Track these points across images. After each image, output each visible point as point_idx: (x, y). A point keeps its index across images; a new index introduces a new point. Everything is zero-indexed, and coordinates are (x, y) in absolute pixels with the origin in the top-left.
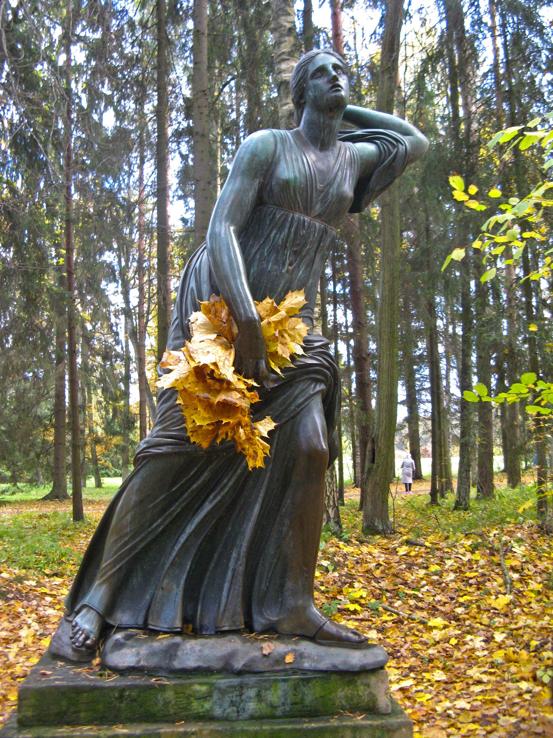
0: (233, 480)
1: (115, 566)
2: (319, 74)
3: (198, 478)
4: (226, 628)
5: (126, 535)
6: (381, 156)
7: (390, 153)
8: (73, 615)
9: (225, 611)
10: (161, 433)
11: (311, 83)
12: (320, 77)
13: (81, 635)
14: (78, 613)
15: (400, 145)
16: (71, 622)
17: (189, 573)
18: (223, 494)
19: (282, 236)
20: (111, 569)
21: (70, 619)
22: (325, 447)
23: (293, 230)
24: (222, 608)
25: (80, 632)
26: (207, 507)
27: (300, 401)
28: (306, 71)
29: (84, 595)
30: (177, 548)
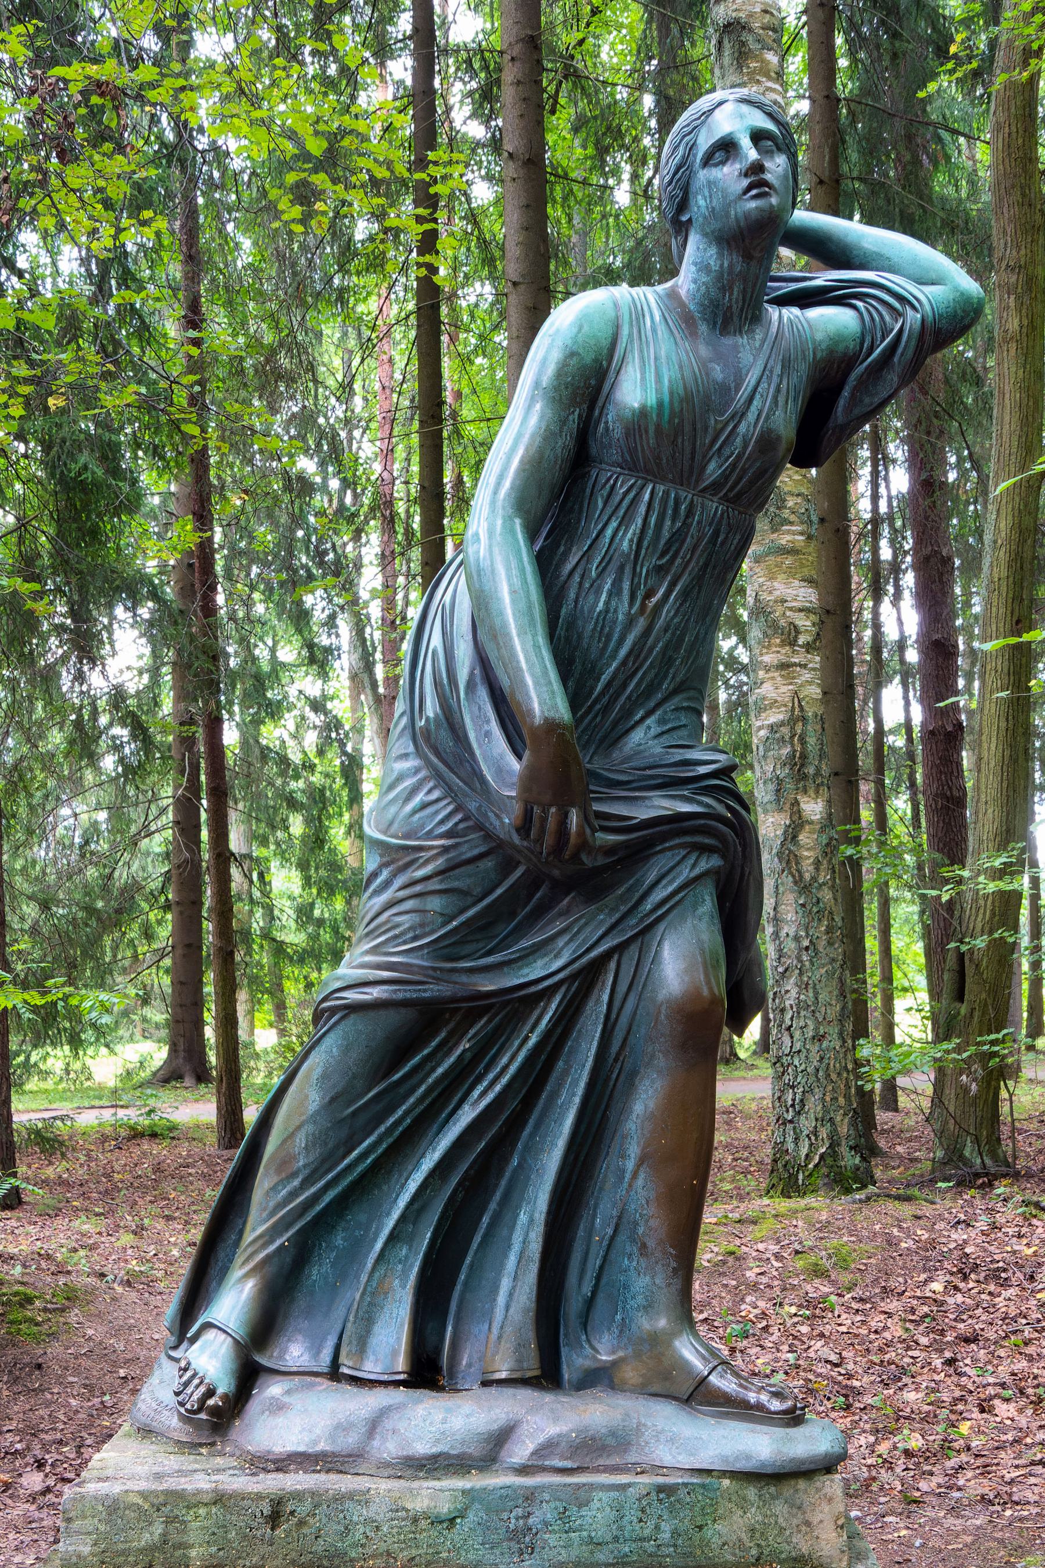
1: (271, 1241)
2: (719, 156)
4: (503, 1375)
5: (294, 1175)
6: (867, 336)
8: (185, 1344)
9: (500, 1337)
10: (368, 958)
11: (703, 175)
12: (723, 163)
13: (197, 1387)
14: (193, 1340)
15: (909, 312)
16: (177, 1360)
19: (629, 535)
20: (264, 1246)
24: (495, 1331)
25: (196, 1381)
28: (692, 147)
29: (208, 1301)
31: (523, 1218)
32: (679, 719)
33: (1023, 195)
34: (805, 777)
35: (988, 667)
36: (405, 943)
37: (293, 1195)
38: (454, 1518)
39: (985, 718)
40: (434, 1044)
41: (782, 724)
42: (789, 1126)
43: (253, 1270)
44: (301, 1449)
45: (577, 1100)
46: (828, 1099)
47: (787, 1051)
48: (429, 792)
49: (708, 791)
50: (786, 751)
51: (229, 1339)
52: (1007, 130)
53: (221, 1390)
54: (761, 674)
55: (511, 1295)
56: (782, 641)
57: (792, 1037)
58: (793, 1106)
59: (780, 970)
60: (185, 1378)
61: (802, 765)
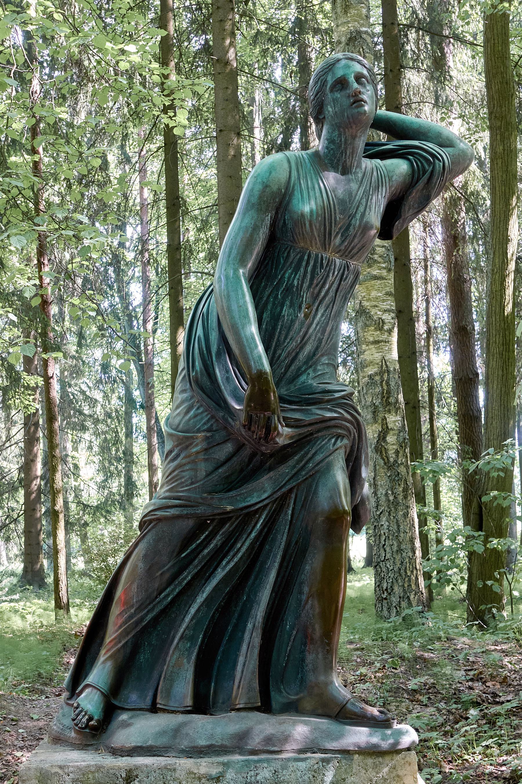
0: (247, 544)
1: (120, 642)
3: (209, 543)
4: (241, 706)
5: (132, 606)
7: (424, 172)
8: (75, 696)
13: (84, 716)
17: (200, 647)
18: (236, 560)
20: (116, 644)
21: (71, 702)
22: (347, 508)
23: (309, 269)
26: (220, 574)
27: (318, 458)
30: (187, 619)
31: (250, 626)
32: (324, 370)
33: (503, 78)
34: (389, 404)
35: (491, 341)
36: (187, 486)
37: (131, 617)
38: (219, 777)
39: (490, 370)
40: (202, 538)
41: (376, 374)
42: (385, 601)
43: (110, 657)
44: (139, 744)
45: (277, 565)
46: (406, 585)
47: (383, 559)
48: (198, 408)
49: (340, 405)
50: (378, 389)
51: (99, 692)
52: (493, 42)
53: (96, 718)
54: (364, 347)
55: (244, 665)
56: (375, 328)
57: (385, 551)
58: (386, 590)
59: (378, 513)
60: (77, 712)
61: (388, 398)
